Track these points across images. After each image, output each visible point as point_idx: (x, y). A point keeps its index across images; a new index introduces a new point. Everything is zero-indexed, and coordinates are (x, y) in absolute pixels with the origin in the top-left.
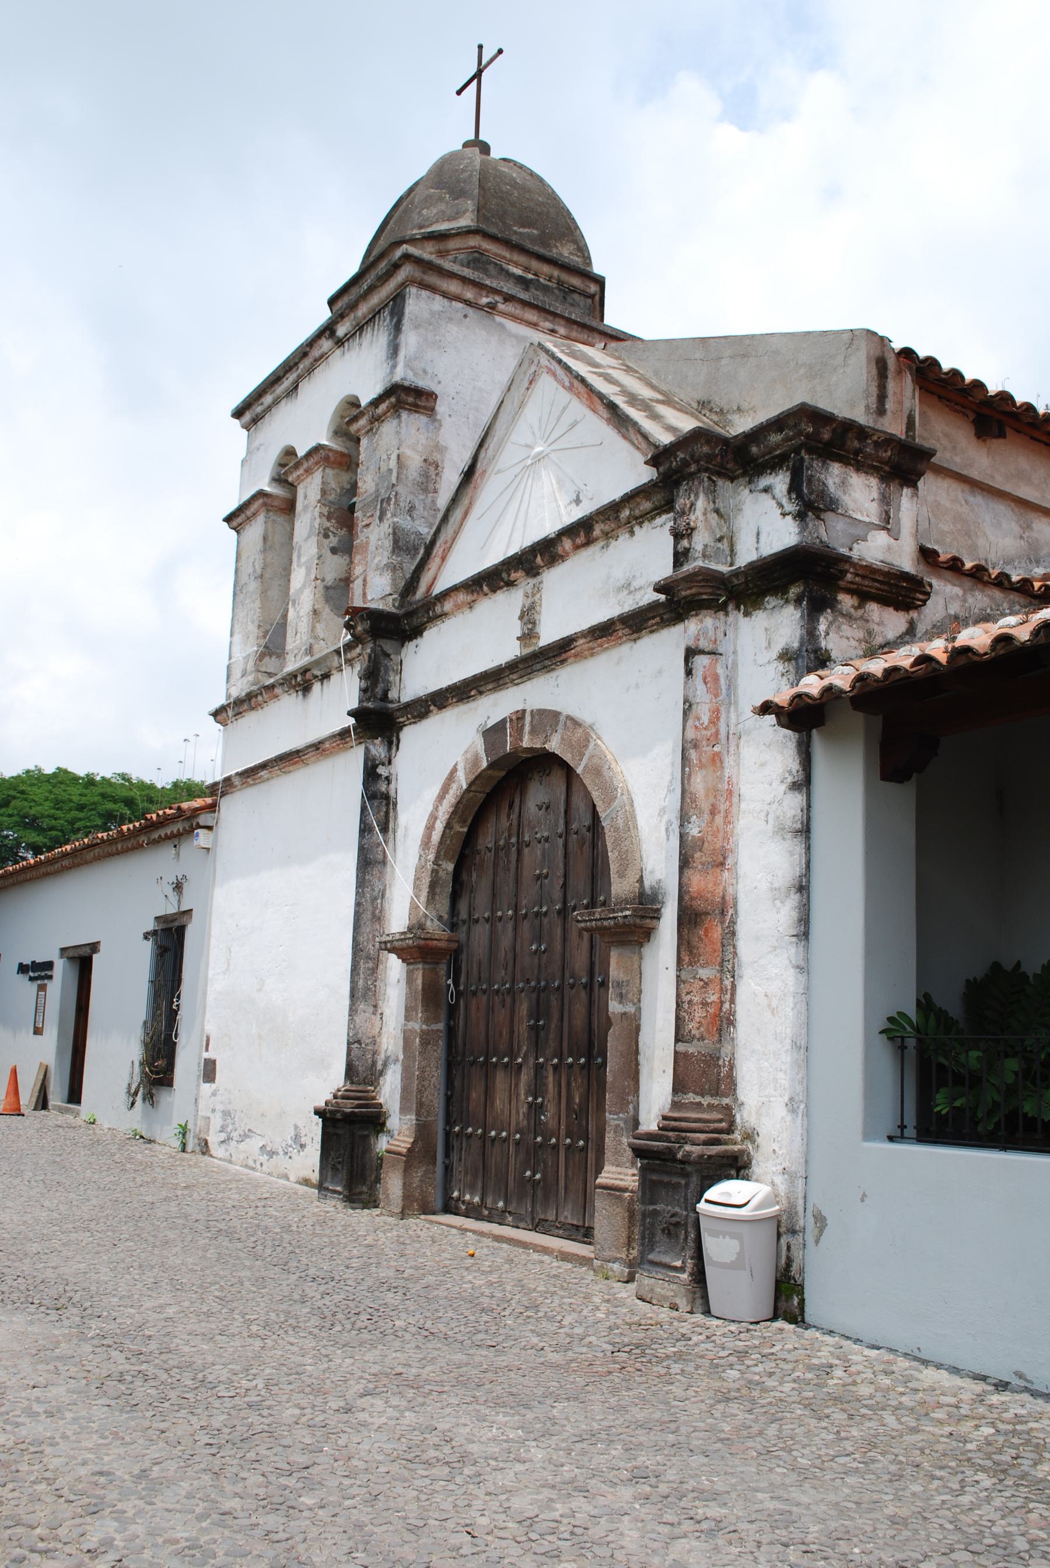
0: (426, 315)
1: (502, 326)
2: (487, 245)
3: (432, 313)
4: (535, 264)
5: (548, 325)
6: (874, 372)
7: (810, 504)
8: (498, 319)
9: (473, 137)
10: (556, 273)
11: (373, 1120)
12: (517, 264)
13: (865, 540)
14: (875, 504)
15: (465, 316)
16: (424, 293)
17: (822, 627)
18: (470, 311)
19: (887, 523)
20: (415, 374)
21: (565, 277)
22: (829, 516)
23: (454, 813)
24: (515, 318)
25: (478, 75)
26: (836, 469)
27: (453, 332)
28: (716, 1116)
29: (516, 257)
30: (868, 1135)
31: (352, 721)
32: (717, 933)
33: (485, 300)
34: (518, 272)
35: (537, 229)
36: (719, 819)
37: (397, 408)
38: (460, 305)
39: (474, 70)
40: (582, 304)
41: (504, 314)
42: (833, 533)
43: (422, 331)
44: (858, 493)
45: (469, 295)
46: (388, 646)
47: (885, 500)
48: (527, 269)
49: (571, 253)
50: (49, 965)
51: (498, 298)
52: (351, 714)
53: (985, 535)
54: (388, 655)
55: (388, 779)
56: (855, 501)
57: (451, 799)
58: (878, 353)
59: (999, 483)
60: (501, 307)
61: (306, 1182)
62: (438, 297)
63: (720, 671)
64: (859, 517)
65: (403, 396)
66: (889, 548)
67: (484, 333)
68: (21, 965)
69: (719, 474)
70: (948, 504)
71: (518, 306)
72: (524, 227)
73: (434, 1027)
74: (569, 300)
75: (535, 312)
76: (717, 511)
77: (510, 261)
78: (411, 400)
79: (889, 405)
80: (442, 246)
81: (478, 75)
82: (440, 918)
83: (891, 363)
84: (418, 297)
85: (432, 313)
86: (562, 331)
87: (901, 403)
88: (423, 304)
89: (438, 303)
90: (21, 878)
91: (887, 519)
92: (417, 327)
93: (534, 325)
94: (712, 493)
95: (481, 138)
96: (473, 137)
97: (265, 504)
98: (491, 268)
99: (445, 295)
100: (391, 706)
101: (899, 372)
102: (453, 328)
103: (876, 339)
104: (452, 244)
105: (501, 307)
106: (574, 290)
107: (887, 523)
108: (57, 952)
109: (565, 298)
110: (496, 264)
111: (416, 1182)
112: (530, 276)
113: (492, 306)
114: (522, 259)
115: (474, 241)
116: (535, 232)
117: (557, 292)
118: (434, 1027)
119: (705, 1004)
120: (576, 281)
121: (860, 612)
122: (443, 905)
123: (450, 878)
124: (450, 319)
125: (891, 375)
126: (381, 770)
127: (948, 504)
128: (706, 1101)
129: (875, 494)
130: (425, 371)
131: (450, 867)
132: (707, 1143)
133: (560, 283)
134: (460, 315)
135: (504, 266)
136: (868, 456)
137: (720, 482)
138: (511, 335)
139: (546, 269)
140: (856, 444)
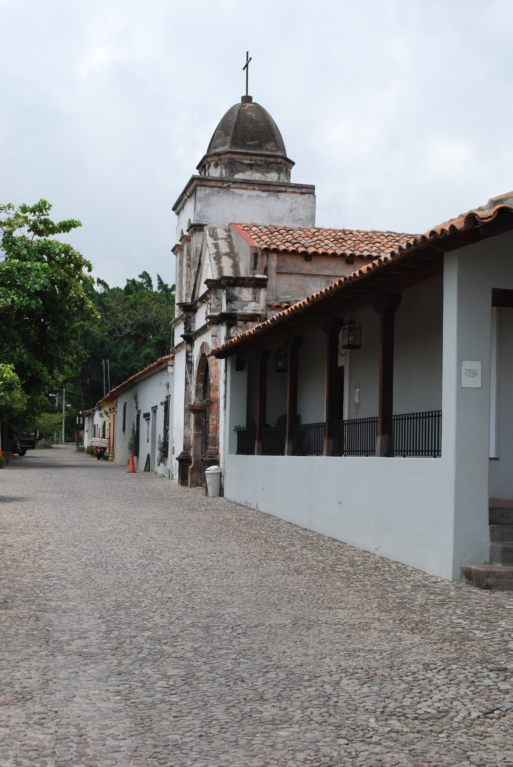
0: (204, 196)
1: (233, 192)
2: (233, 156)
3: (206, 195)
4: (254, 158)
5: (251, 187)
6: (253, 257)
8: (232, 190)
9: (245, 95)
10: (263, 159)
11: (189, 461)
12: (247, 159)
13: (247, 305)
14: (251, 295)
15: (219, 192)
16: (203, 188)
17: (232, 331)
18: (221, 190)
19: (255, 299)
20: (200, 218)
22: (235, 302)
23: (198, 370)
24: (238, 188)
26: (237, 289)
27: (214, 199)
28: (214, 451)
29: (246, 157)
30: (230, 453)
32: (216, 407)
33: (225, 185)
34: (248, 162)
35: (257, 140)
36: (217, 379)
37: (195, 230)
38: (217, 189)
40: (276, 167)
41: (233, 188)
43: (202, 202)
44: (246, 294)
45: (219, 185)
46: (190, 314)
47: (254, 293)
48: (251, 160)
49: (272, 147)
51: (230, 183)
53: (310, 288)
54: (190, 317)
55: (191, 357)
56: (244, 296)
58: (254, 252)
59: (314, 272)
60: (232, 186)
61: (486, 563)
62: (208, 188)
63: (217, 341)
64: (245, 300)
65: (195, 228)
66: (256, 306)
67: (226, 196)
69: (218, 288)
70: (295, 282)
71: (238, 184)
72: (252, 141)
73: (199, 432)
74: (270, 167)
75: (245, 184)
76: (217, 298)
77: (244, 159)
78: (198, 228)
79: (258, 266)
80: (219, 158)
83: (259, 253)
84: (200, 190)
85: (206, 195)
86: (257, 188)
87: (262, 264)
88: (202, 192)
89: (208, 190)
90: (143, 377)
91: (255, 298)
92: (200, 201)
93: (246, 189)
94: (216, 293)
95: (248, 95)
96: (245, 95)
97: (179, 249)
98: (237, 164)
99: (210, 187)
100: (191, 333)
101: (262, 255)
102: (214, 198)
103: (254, 248)
104: (223, 157)
105: (232, 186)
106: (272, 163)
107: (255, 299)
108: (150, 409)
109: (268, 167)
110: (238, 162)
111: (194, 477)
112: (253, 162)
113: (229, 187)
114: (249, 157)
115: (229, 156)
116: (257, 142)
117: (265, 165)
118: (199, 432)
119: (213, 424)
120: (272, 160)
121: (245, 325)
122: (201, 396)
123: (202, 388)
124: (213, 195)
125: (259, 257)
126: (189, 354)
127: (295, 282)
128: (213, 447)
129: (251, 292)
130: (204, 216)
131: (202, 385)
132: (209, 457)
133: (265, 161)
134: (216, 192)
135: (242, 161)
136: (247, 284)
137: (218, 290)
138: (237, 194)
139: (259, 158)
140: (242, 282)
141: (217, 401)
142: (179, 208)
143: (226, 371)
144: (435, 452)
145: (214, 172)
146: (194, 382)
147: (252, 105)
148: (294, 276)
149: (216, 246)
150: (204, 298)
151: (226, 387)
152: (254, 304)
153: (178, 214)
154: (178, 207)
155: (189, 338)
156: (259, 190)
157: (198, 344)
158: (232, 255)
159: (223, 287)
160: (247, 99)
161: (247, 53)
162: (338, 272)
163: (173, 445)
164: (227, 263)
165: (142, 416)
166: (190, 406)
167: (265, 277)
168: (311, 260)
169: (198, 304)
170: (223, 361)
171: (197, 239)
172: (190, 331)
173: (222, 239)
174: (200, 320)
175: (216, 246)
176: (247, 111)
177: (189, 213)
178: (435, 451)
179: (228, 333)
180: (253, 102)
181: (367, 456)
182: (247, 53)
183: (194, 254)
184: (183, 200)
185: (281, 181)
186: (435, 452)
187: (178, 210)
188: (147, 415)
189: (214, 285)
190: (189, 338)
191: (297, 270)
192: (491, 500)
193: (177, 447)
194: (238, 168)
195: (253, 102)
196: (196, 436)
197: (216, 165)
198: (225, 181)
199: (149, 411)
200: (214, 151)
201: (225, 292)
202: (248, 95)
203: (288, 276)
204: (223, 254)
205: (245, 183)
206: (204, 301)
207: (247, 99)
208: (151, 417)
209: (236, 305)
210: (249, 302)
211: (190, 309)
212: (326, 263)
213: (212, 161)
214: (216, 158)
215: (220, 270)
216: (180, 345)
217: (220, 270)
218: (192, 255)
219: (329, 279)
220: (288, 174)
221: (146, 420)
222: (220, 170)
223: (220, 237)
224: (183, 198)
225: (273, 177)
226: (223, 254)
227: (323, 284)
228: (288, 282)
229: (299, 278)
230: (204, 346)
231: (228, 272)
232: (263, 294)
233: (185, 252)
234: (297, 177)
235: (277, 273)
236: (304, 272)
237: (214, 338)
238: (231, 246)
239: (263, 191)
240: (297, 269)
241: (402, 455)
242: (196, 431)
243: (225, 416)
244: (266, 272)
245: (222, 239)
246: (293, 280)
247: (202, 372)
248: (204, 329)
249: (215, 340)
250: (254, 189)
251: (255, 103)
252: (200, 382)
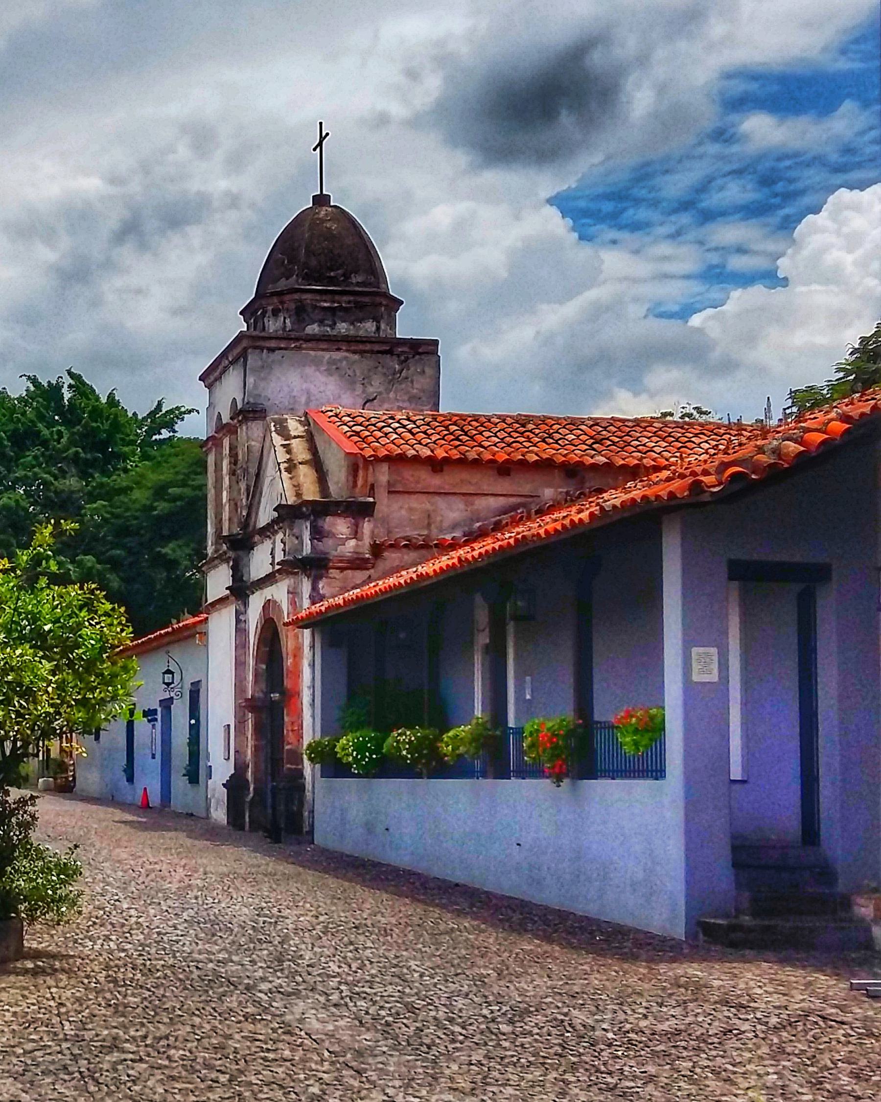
4: (337, 297)
7: (318, 534)
9: (319, 193)
10: (352, 298)
12: (325, 301)
21: (359, 299)
22: (325, 540)
24: (313, 349)
25: (320, 144)
29: (324, 298)
31: (228, 592)
37: (246, 419)
39: (318, 141)
42: (327, 545)
44: (341, 526)
46: (240, 553)
47: (357, 525)
50: (156, 710)
52: (227, 589)
57: (257, 637)
66: (357, 545)
68: (144, 711)
78: (251, 415)
81: (320, 144)
82: (262, 691)
87: (366, 481)
91: (356, 532)
95: (324, 192)
96: (319, 193)
104: (287, 298)
107: (356, 534)
112: (336, 305)
114: (329, 297)
120: (366, 299)
131: (264, 667)
133: (356, 303)
141: (298, 694)
142: (212, 378)
143: (312, 647)
144: (658, 772)
145: (273, 325)
146: (251, 662)
147: (330, 209)
148: (416, 496)
149: (288, 449)
150: (268, 531)
151: (314, 672)
152: (353, 543)
153: (209, 387)
154: (211, 377)
155: (240, 590)
156: (347, 351)
157: (256, 602)
158: (317, 463)
159: (305, 517)
160: (321, 200)
161: (321, 124)
162: (485, 487)
163: (209, 764)
164: (306, 475)
165: (138, 714)
166: (247, 700)
167: (371, 500)
168: (442, 471)
169: (257, 538)
170: (307, 632)
171: (251, 434)
172: (241, 579)
173: (295, 437)
174: (260, 562)
175: (288, 449)
176: (323, 221)
177: (231, 388)
178: (656, 771)
179: (314, 588)
180: (332, 204)
181: (613, 779)
182: (321, 124)
183: (243, 456)
184: (221, 367)
185: (382, 334)
186: (658, 772)
187: (210, 381)
188: (149, 714)
189: (288, 515)
190: (240, 590)
191: (419, 487)
192: (734, 837)
193: (220, 767)
194: (311, 315)
195: (332, 204)
196: (257, 749)
197: (275, 313)
198: (291, 339)
199: (156, 706)
200: (271, 289)
201: (308, 524)
202: (324, 192)
203: (406, 496)
204: (300, 463)
205: (326, 340)
206: (268, 534)
207: (321, 200)
208: (159, 717)
209: (327, 545)
210: (344, 537)
211: (241, 544)
212: (465, 475)
213: (269, 304)
214: (275, 300)
215: (297, 487)
216: (222, 601)
217: (297, 487)
218: (240, 457)
219: (470, 499)
220: (392, 324)
221: (149, 721)
222: (282, 319)
223: (293, 433)
224: (220, 363)
225: (368, 327)
226: (300, 463)
227: (462, 506)
228: (406, 506)
229: (423, 497)
230: (269, 605)
231: (311, 493)
232: (367, 527)
233: (226, 451)
234: (405, 328)
235: (389, 492)
236: (431, 490)
237: (291, 596)
238: (313, 449)
239: (355, 352)
240: (419, 486)
241: (652, 777)
242: (256, 740)
243: (313, 717)
244: (372, 493)
245: (295, 437)
246: (414, 502)
247: (265, 646)
248: (269, 580)
249: (294, 598)
250: (339, 349)
251: (335, 206)
252: (262, 663)
